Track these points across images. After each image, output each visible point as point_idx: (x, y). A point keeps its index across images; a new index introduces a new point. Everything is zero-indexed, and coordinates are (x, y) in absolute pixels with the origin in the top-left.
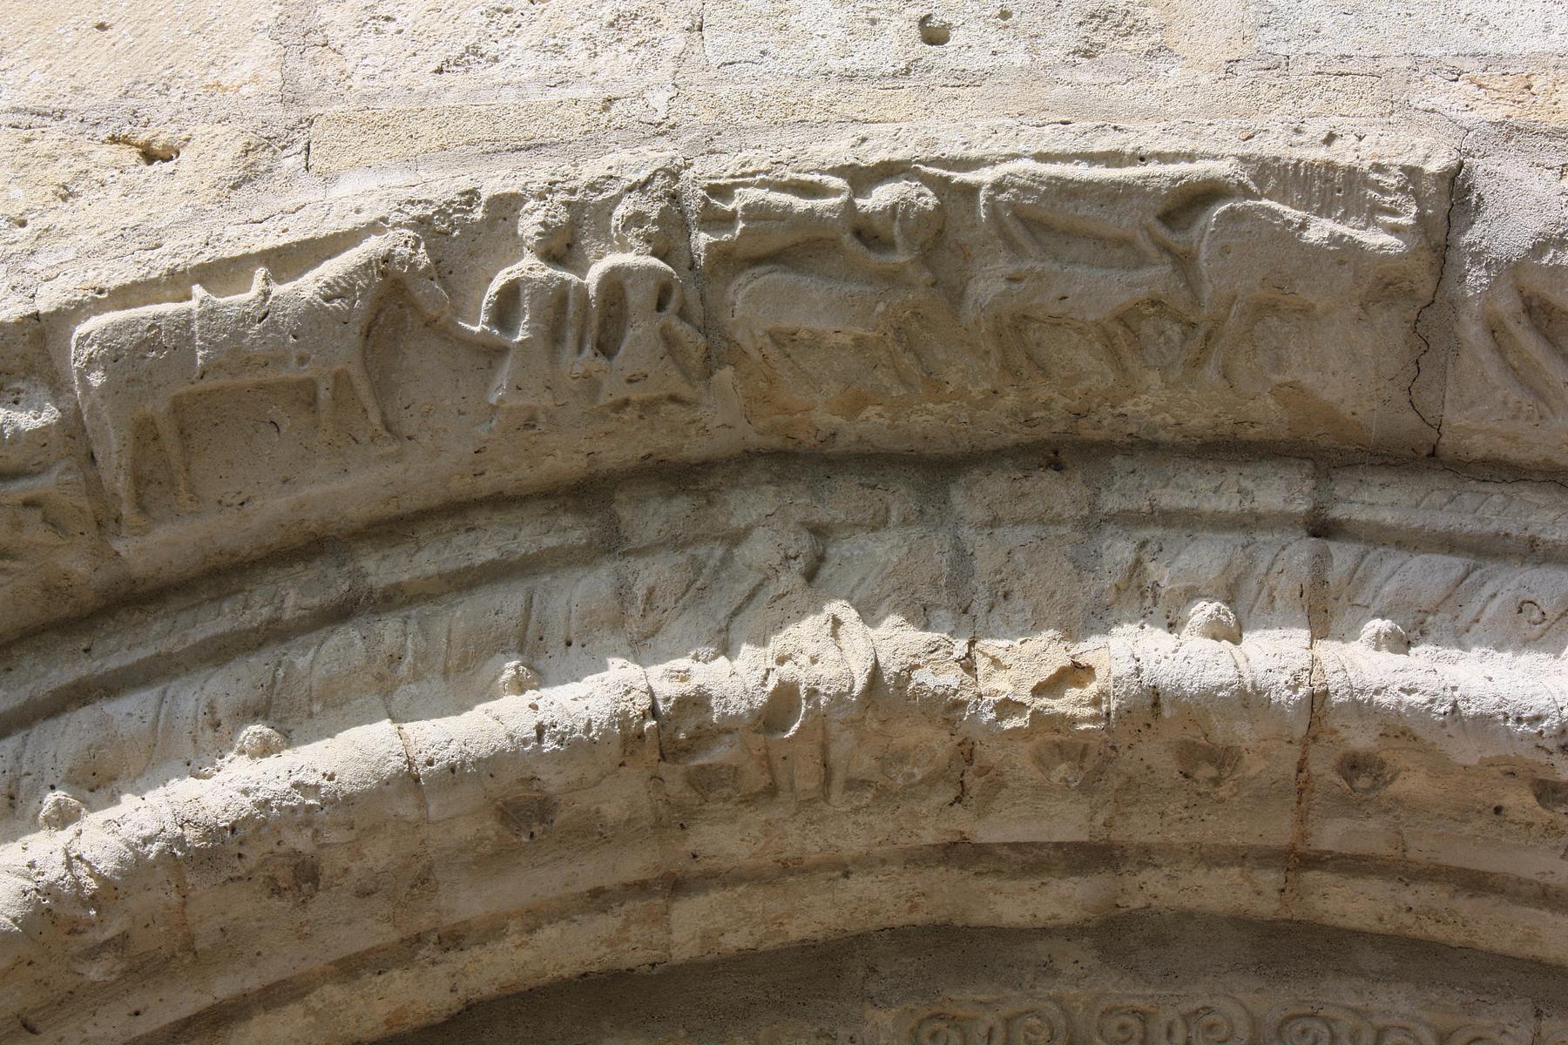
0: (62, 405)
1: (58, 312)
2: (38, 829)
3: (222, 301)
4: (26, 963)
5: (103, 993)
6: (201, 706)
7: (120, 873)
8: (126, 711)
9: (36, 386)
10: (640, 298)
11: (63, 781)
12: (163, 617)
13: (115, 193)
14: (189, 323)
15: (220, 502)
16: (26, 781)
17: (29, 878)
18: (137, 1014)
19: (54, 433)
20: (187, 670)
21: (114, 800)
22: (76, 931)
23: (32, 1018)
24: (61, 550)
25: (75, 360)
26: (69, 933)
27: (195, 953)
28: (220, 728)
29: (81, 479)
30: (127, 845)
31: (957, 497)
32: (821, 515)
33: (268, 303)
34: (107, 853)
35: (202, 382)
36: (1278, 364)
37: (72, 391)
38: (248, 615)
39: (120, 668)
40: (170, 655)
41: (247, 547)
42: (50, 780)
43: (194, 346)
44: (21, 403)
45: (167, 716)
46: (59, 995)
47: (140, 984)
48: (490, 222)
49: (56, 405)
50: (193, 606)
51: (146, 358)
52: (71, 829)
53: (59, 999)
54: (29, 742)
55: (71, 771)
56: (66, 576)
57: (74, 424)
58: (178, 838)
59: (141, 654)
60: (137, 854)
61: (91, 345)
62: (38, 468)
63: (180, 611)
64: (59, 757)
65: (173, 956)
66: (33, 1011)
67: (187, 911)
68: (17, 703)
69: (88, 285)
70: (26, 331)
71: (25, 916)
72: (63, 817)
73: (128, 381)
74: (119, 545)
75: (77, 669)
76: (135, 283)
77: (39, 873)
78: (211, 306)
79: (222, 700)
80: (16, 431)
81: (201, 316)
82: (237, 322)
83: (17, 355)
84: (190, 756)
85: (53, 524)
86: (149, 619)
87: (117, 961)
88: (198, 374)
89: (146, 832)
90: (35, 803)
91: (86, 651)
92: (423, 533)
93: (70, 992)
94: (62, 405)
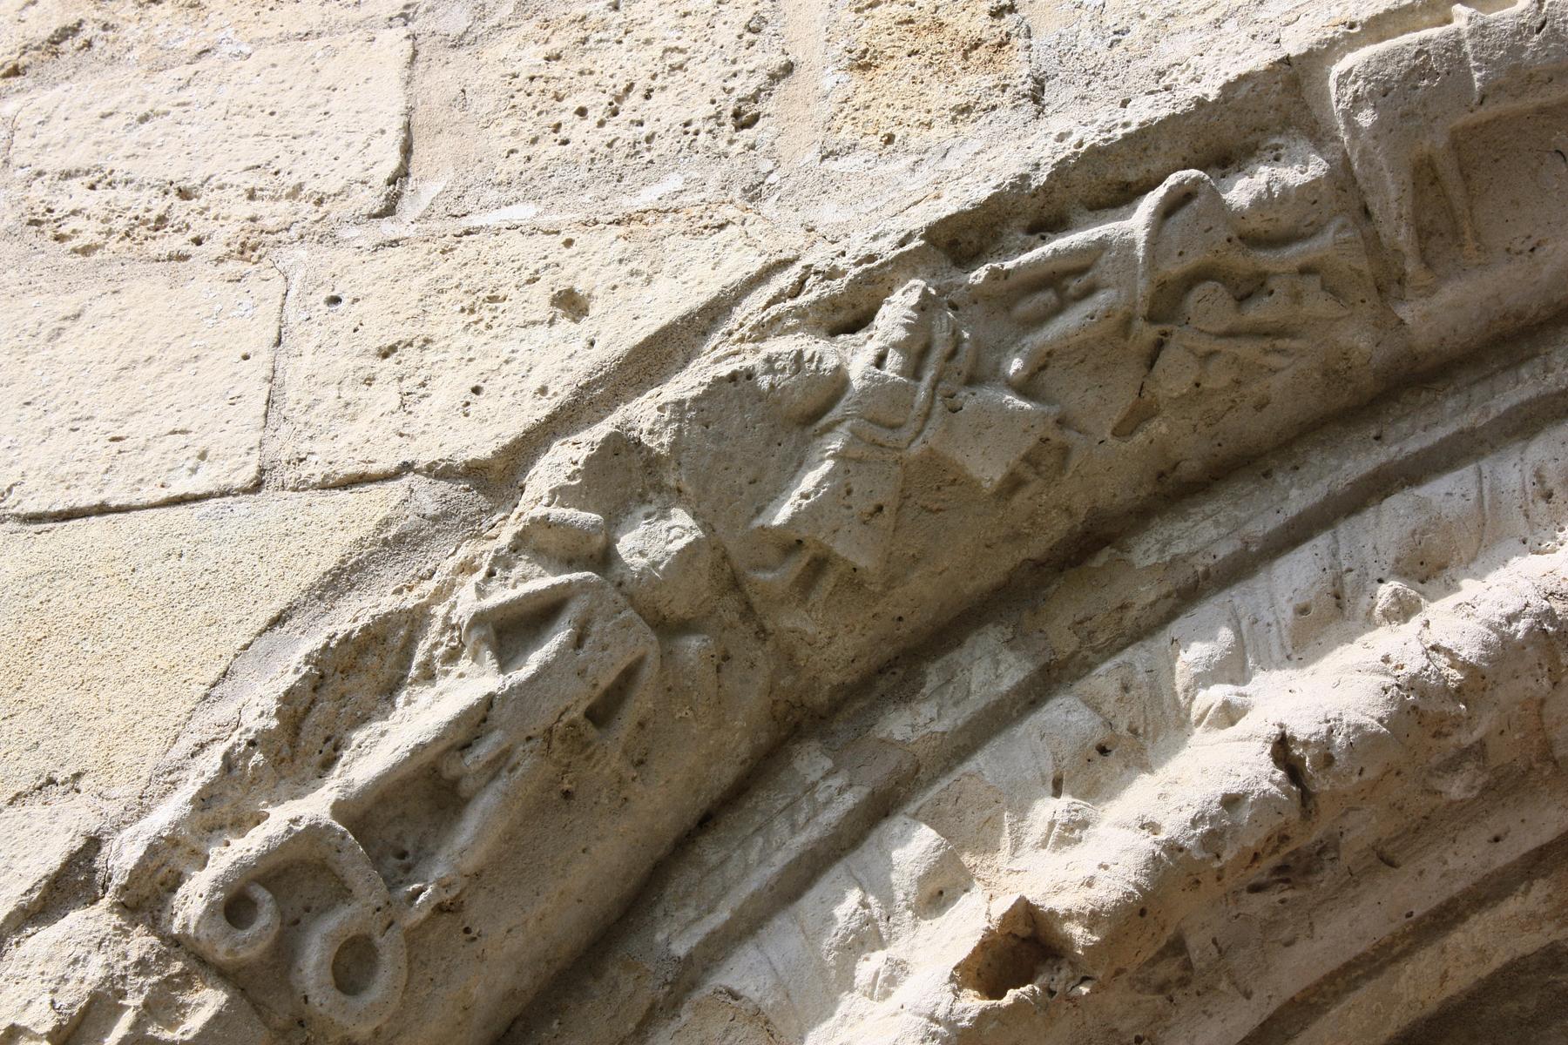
0: (1328, 156)
1: (1310, 53)
2: (1376, 626)
3: (1493, 16)
4: (1394, 772)
5: (1463, 814)
6: (1527, 476)
7: (1487, 659)
8: (1443, 491)
9: (1295, 140)
11: (1391, 573)
12: (1454, 394)
14: (1458, 44)
15: (1508, 250)
16: (1349, 578)
17: (1386, 674)
18: (1497, 840)
19: (1324, 187)
20: (1492, 447)
21: (1451, 587)
22: (1440, 733)
23: (1389, 849)
24: (1342, 322)
25: (1338, 101)
26: (1434, 736)
27: (1555, 762)
28: (1553, 499)
29: (1359, 237)
30: (1489, 627)
33: (1544, 10)
34: (1467, 638)
35: (1482, 109)
37: (1336, 139)
38: (1551, 378)
39: (1422, 450)
40: (1473, 431)
41: (1534, 306)
42: (1375, 573)
43: (1469, 69)
44: (1283, 160)
45: (1491, 490)
46: (1414, 821)
47: (1500, 803)
49: (1321, 154)
50: (1485, 378)
51: (1417, 88)
52: (1416, 622)
53: (1414, 825)
54: (1340, 539)
55: (1398, 560)
56: (1345, 355)
57: (1343, 175)
58: (1547, 611)
59: (1441, 433)
60: (1502, 636)
61: (1354, 82)
62: (1311, 229)
63: (1471, 384)
64: (1381, 548)
65: (1531, 768)
66: (1389, 842)
67: (1545, 711)
68: (1317, 499)
69: (1337, 21)
70: (1279, 77)
71: (1391, 715)
72: (1403, 610)
73: (1402, 116)
74: (1405, 312)
75: (1374, 457)
76: (1388, 12)
77: (1396, 667)
78: (1481, 22)
79: (1551, 465)
80: (1284, 188)
81: (1472, 34)
82: (1513, 35)
83: (1271, 107)
84: (1524, 531)
85: (1334, 292)
86: (1439, 398)
87: (1478, 772)
88: (1477, 99)
89: (1509, 610)
90: (1364, 601)
91: (1377, 438)
93: (1425, 818)
94: (1328, 156)
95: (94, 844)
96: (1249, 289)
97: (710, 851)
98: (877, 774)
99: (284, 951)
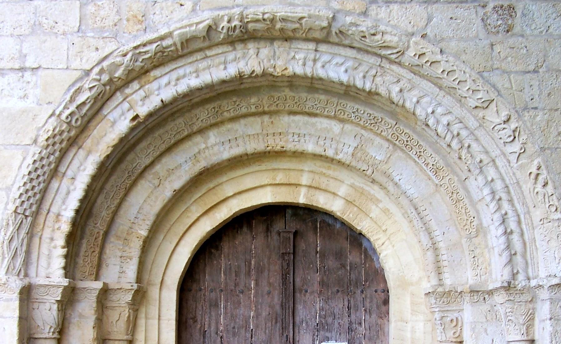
10: (238, 27)
13: (178, 12)
31: (275, 44)
32: (259, 47)
36: (312, 35)
48: (221, 18)
92: (213, 48)
95: (54, 111)
96: (163, 52)
97: (108, 103)
98: (125, 96)
99: (71, 121)
